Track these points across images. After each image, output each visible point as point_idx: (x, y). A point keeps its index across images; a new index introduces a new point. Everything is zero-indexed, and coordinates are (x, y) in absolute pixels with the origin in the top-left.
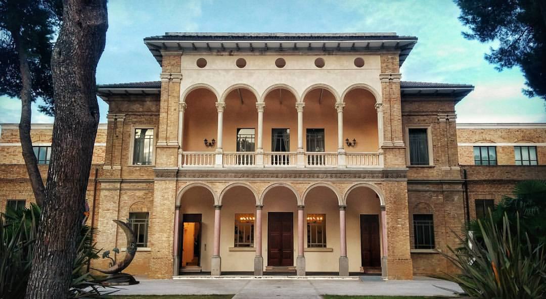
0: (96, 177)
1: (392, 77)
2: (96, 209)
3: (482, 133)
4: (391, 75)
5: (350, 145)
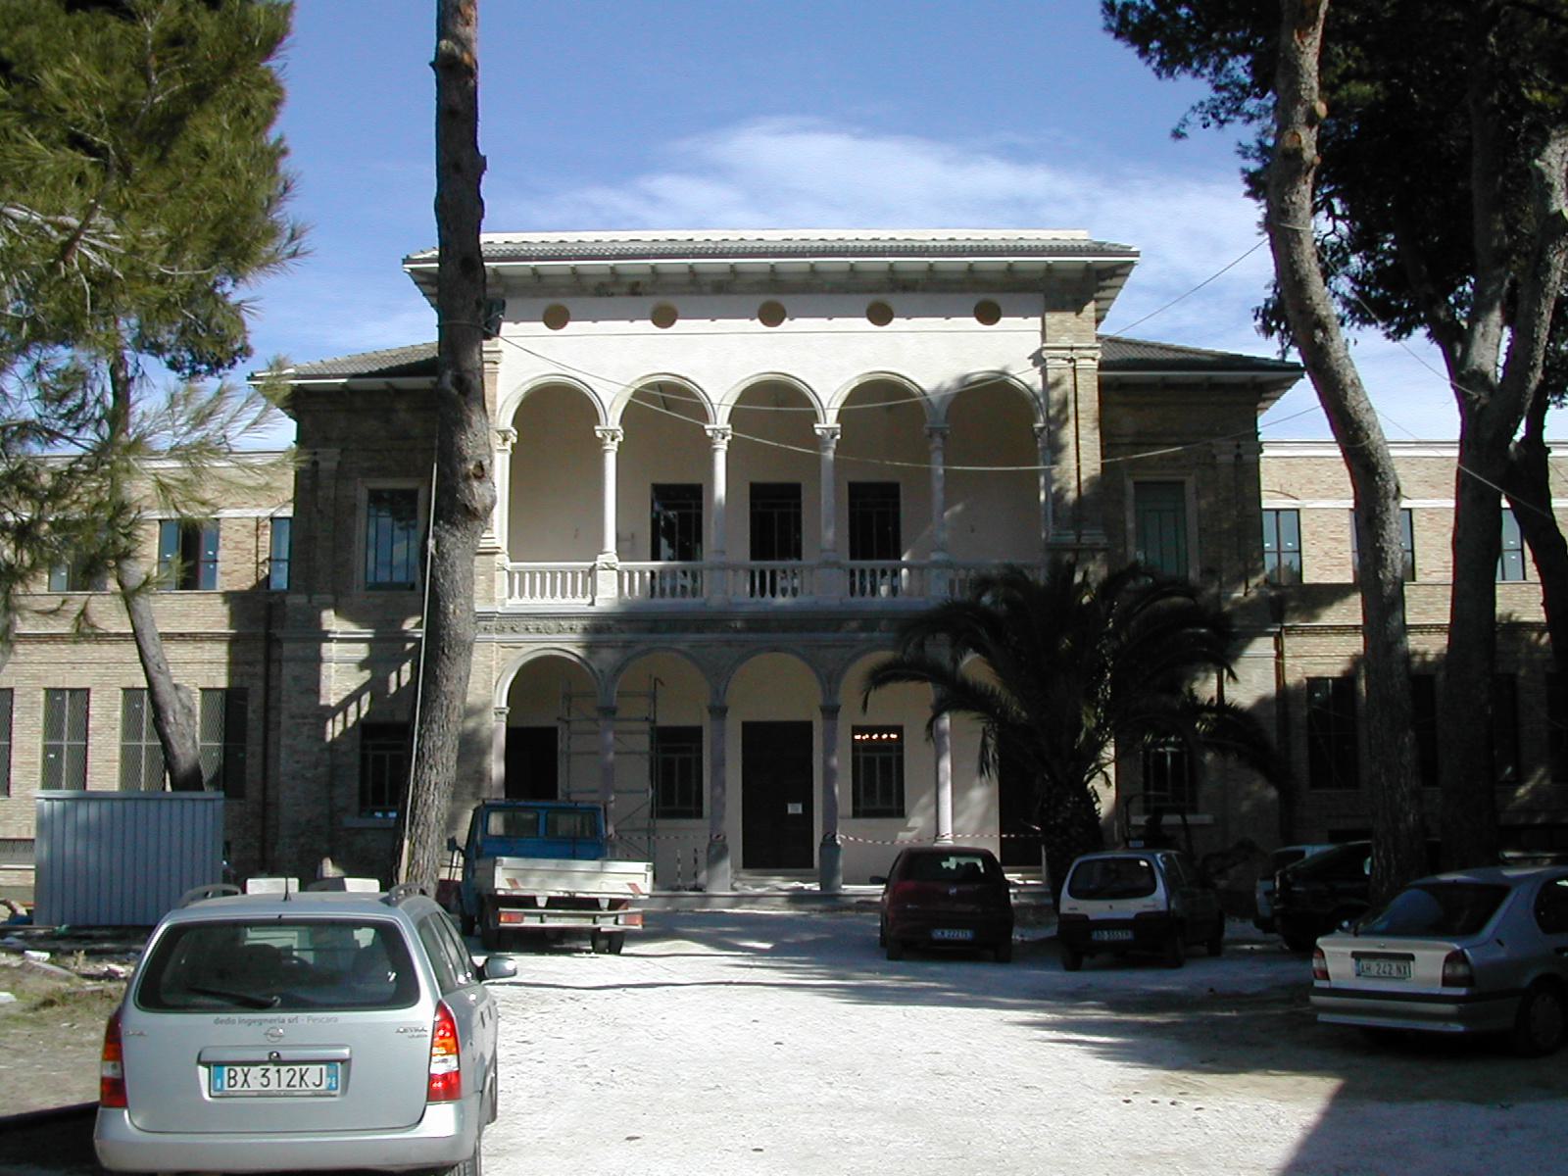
0: (269, 625)
1: (1074, 354)
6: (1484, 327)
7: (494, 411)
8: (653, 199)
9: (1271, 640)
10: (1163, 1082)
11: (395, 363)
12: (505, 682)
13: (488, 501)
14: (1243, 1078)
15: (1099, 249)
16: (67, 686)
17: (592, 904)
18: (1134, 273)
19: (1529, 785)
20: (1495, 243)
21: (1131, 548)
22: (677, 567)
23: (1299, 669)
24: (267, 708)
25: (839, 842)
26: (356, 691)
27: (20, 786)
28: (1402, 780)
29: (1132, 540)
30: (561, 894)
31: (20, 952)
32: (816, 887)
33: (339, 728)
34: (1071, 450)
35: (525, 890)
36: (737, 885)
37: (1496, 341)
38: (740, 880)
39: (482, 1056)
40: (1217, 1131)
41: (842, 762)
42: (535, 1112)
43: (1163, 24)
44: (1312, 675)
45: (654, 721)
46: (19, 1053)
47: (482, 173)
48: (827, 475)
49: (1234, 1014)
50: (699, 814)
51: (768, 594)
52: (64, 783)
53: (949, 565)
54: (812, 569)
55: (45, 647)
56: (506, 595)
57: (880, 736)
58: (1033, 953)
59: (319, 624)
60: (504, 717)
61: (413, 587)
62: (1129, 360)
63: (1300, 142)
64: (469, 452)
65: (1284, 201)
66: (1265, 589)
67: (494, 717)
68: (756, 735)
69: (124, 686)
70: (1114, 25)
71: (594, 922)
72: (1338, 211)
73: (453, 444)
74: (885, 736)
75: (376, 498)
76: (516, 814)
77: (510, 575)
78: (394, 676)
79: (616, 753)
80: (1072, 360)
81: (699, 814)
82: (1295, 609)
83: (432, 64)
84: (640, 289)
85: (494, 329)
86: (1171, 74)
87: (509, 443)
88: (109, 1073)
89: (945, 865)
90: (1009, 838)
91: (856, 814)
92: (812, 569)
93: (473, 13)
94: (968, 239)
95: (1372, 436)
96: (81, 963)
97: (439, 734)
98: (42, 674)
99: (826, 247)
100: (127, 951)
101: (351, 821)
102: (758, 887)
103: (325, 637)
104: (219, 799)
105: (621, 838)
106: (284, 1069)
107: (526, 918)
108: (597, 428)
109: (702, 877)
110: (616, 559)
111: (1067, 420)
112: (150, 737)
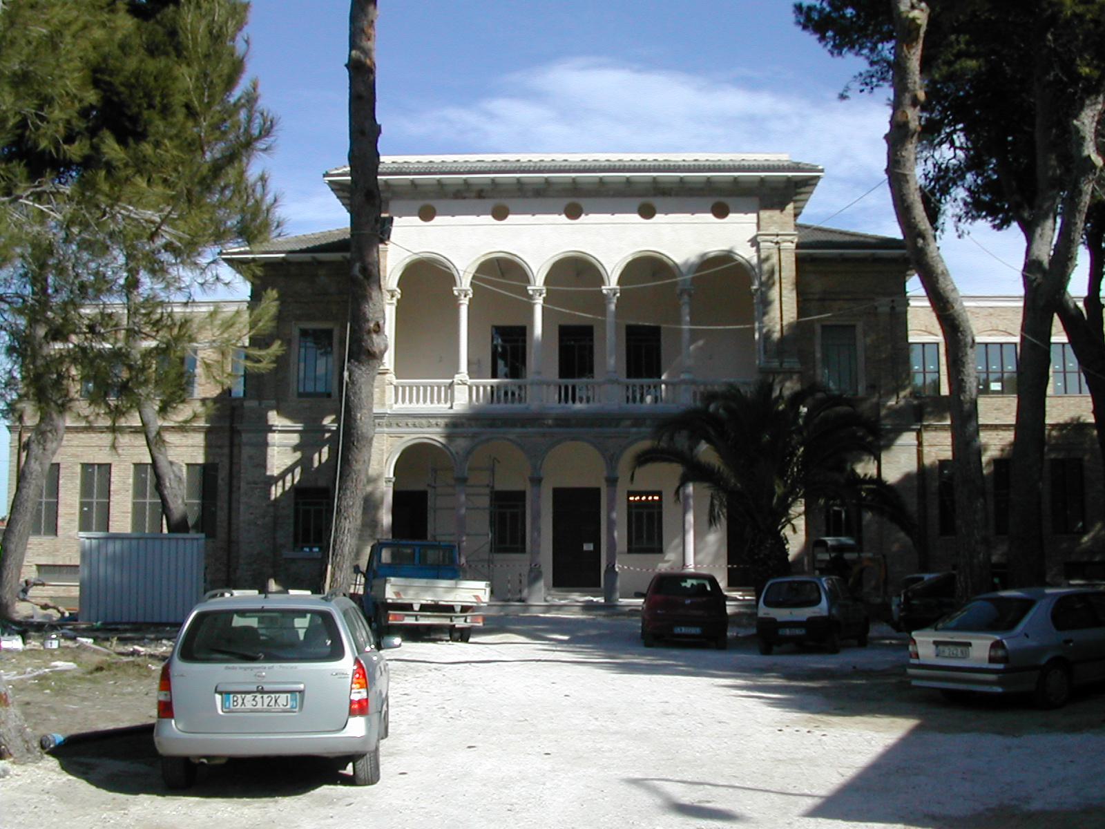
0: (232, 422)
1: (778, 239)
3: (991, 315)
4: (777, 235)
5: (59, 31)
6: (1042, 230)
7: (385, 277)
8: (492, 116)
9: (914, 434)
10: (806, 721)
11: (317, 243)
12: (392, 460)
13: (383, 347)
14: (858, 719)
15: (797, 167)
16: (96, 462)
17: (450, 609)
18: (820, 183)
19: (1092, 534)
20: (1050, 173)
21: (819, 371)
22: (508, 383)
23: (933, 454)
24: (231, 475)
25: (617, 570)
26: (291, 466)
27: (65, 529)
28: (976, 531)
29: (819, 365)
30: (429, 602)
31: (74, 639)
32: (601, 600)
33: (280, 491)
34: (776, 304)
35: (405, 599)
36: (549, 598)
37: (1049, 239)
38: (549, 595)
39: (381, 693)
40: (832, 748)
41: (620, 515)
42: (411, 733)
43: (834, 20)
44: (942, 458)
45: (493, 487)
46: (84, 699)
47: (378, 135)
48: (610, 319)
49: (864, 682)
50: (523, 550)
51: (570, 402)
52: (94, 527)
53: (693, 382)
54: (600, 385)
55: (81, 435)
56: (393, 401)
57: (647, 498)
58: (741, 644)
59: (266, 421)
60: (391, 484)
61: (329, 395)
62: (818, 241)
63: (907, 117)
64: (370, 316)
65: (897, 155)
66: (911, 400)
67: (384, 484)
68: (562, 498)
69: (135, 462)
70: (802, 20)
71: (451, 621)
72: (957, 144)
73: (360, 310)
74: (650, 498)
75: (304, 333)
76: (400, 549)
77: (396, 388)
78: (316, 456)
79: (467, 509)
80: (777, 243)
81: (523, 550)
82: (930, 413)
83: (346, 65)
84: (484, 194)
85: (386, 236)
86: (840, 53)
87: (395, 299)
88: (162, 698)
89: (683, 584)
90: (732, 567)
91: (630, 550)
92: (600, 385)
93: (373, 32)
94: (707, 160)
95: (956, 307)
96: (114, 645)
97: (351, 497)
98: (79, 453)
99: (610, 166)
100: (143, 638)
101: (288, 554)
102: (562, 599)
103: (270, 429)
104: (201, 539)
105: (470, 566)
106: (265, 696)
107: (406, 618)
108: (454, 288)
109: (525, 593)
110: (467, 378)
111: (774, 284)
112: (153, 496)
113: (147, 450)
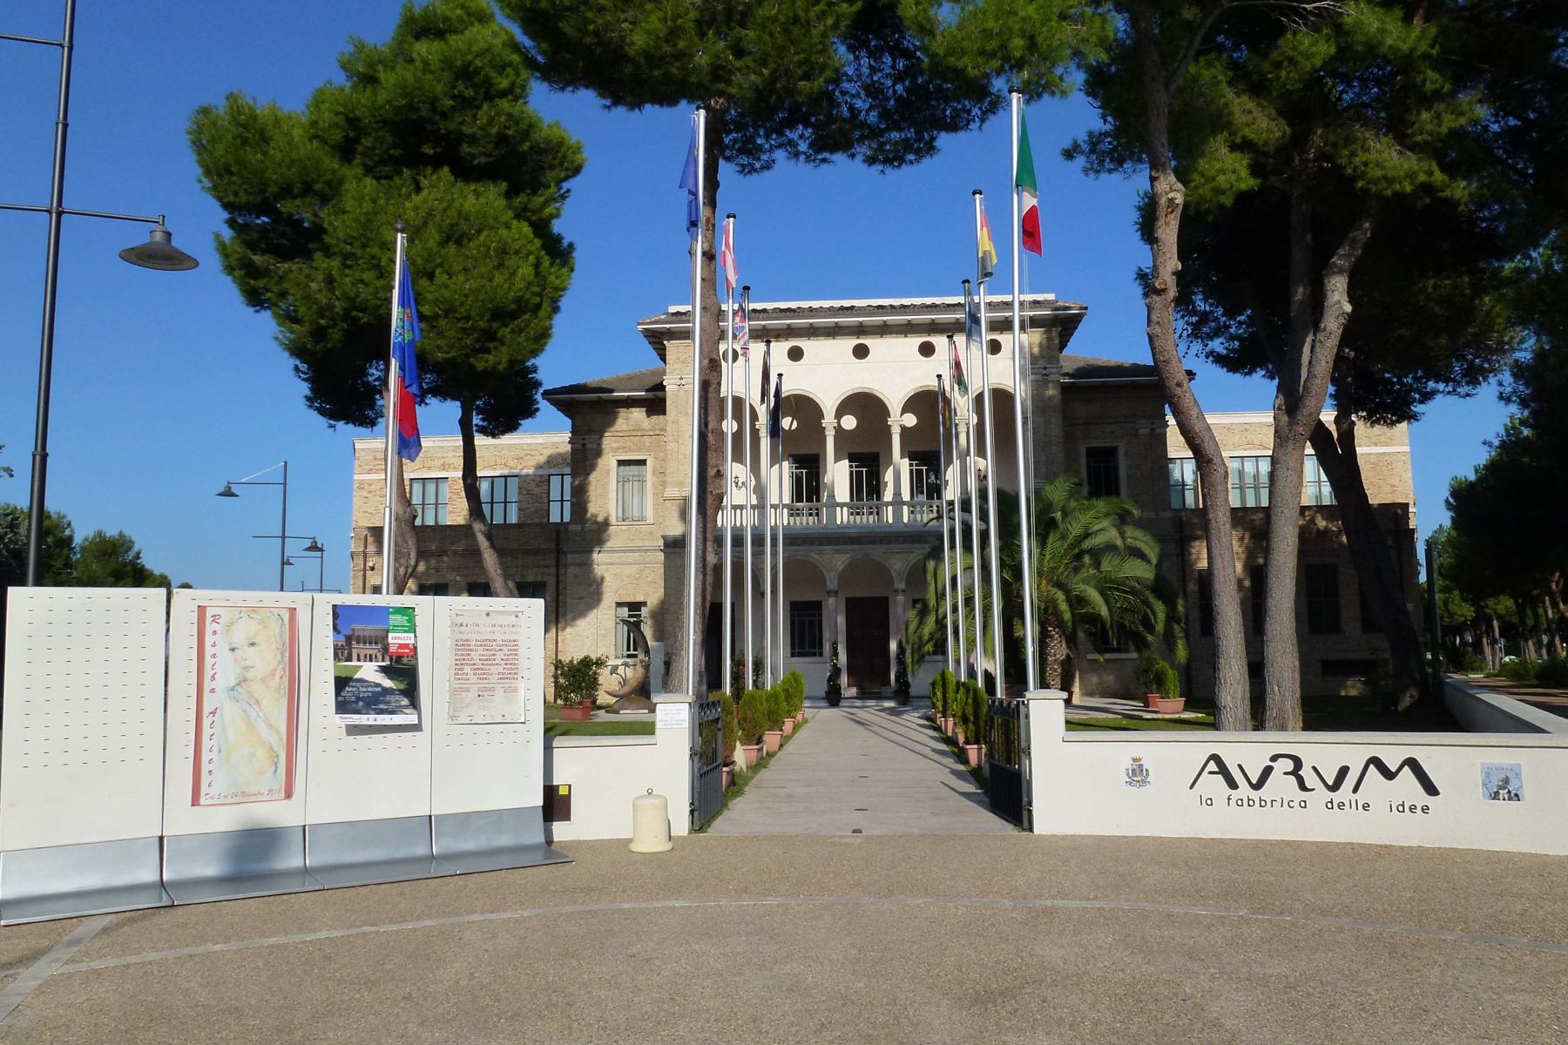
0: (558, 544)
2: (561, 598)
113: (458, 441)
